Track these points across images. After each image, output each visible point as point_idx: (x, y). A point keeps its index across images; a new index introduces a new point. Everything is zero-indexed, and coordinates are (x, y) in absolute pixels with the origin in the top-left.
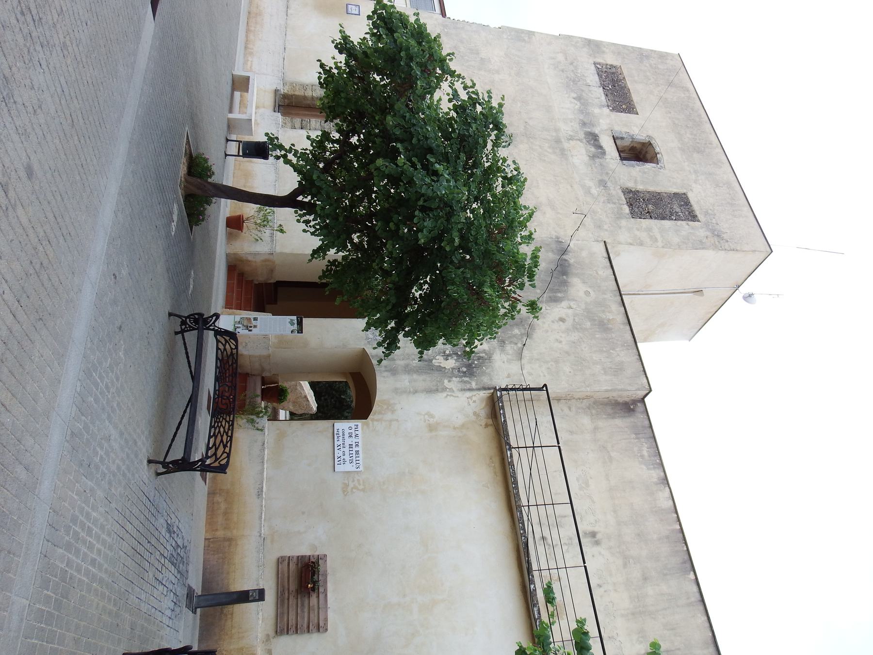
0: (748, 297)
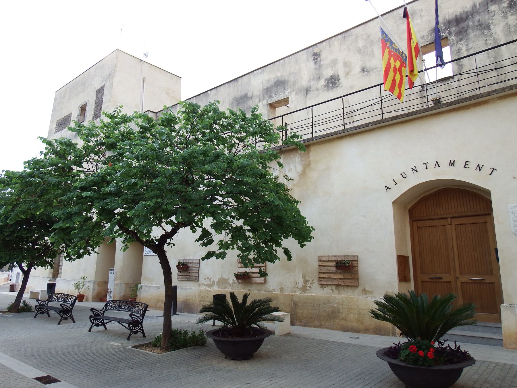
0: (146, 55)
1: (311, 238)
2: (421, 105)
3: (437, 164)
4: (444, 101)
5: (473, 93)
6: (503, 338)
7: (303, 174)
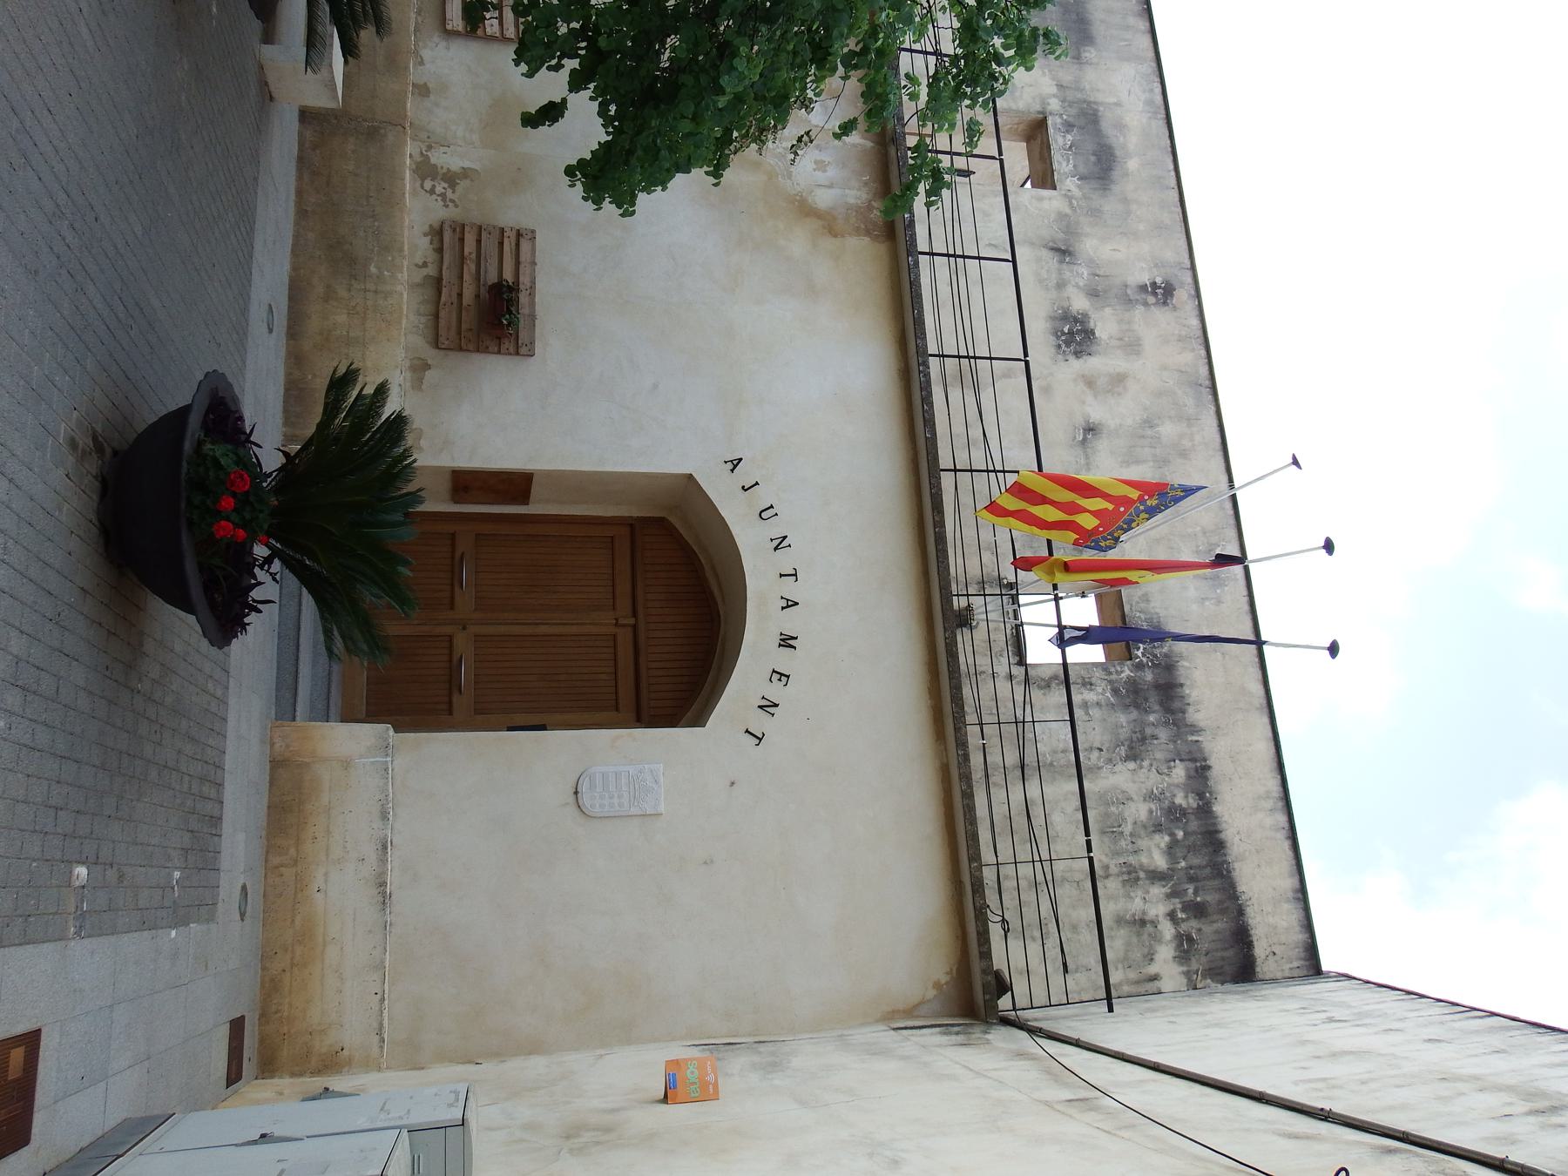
1: (598, 202)
2: (961, 579)
3: (791, 604)
4: (963, 637)
5: (969, 708)
6: (299, 722)
7: (804, 209)
